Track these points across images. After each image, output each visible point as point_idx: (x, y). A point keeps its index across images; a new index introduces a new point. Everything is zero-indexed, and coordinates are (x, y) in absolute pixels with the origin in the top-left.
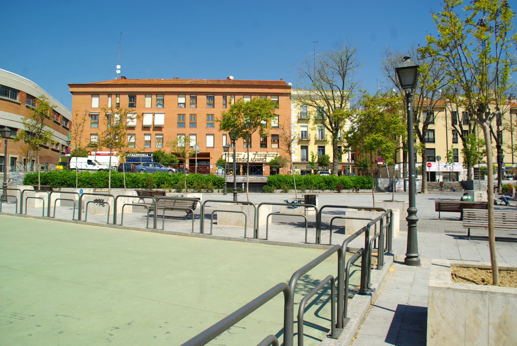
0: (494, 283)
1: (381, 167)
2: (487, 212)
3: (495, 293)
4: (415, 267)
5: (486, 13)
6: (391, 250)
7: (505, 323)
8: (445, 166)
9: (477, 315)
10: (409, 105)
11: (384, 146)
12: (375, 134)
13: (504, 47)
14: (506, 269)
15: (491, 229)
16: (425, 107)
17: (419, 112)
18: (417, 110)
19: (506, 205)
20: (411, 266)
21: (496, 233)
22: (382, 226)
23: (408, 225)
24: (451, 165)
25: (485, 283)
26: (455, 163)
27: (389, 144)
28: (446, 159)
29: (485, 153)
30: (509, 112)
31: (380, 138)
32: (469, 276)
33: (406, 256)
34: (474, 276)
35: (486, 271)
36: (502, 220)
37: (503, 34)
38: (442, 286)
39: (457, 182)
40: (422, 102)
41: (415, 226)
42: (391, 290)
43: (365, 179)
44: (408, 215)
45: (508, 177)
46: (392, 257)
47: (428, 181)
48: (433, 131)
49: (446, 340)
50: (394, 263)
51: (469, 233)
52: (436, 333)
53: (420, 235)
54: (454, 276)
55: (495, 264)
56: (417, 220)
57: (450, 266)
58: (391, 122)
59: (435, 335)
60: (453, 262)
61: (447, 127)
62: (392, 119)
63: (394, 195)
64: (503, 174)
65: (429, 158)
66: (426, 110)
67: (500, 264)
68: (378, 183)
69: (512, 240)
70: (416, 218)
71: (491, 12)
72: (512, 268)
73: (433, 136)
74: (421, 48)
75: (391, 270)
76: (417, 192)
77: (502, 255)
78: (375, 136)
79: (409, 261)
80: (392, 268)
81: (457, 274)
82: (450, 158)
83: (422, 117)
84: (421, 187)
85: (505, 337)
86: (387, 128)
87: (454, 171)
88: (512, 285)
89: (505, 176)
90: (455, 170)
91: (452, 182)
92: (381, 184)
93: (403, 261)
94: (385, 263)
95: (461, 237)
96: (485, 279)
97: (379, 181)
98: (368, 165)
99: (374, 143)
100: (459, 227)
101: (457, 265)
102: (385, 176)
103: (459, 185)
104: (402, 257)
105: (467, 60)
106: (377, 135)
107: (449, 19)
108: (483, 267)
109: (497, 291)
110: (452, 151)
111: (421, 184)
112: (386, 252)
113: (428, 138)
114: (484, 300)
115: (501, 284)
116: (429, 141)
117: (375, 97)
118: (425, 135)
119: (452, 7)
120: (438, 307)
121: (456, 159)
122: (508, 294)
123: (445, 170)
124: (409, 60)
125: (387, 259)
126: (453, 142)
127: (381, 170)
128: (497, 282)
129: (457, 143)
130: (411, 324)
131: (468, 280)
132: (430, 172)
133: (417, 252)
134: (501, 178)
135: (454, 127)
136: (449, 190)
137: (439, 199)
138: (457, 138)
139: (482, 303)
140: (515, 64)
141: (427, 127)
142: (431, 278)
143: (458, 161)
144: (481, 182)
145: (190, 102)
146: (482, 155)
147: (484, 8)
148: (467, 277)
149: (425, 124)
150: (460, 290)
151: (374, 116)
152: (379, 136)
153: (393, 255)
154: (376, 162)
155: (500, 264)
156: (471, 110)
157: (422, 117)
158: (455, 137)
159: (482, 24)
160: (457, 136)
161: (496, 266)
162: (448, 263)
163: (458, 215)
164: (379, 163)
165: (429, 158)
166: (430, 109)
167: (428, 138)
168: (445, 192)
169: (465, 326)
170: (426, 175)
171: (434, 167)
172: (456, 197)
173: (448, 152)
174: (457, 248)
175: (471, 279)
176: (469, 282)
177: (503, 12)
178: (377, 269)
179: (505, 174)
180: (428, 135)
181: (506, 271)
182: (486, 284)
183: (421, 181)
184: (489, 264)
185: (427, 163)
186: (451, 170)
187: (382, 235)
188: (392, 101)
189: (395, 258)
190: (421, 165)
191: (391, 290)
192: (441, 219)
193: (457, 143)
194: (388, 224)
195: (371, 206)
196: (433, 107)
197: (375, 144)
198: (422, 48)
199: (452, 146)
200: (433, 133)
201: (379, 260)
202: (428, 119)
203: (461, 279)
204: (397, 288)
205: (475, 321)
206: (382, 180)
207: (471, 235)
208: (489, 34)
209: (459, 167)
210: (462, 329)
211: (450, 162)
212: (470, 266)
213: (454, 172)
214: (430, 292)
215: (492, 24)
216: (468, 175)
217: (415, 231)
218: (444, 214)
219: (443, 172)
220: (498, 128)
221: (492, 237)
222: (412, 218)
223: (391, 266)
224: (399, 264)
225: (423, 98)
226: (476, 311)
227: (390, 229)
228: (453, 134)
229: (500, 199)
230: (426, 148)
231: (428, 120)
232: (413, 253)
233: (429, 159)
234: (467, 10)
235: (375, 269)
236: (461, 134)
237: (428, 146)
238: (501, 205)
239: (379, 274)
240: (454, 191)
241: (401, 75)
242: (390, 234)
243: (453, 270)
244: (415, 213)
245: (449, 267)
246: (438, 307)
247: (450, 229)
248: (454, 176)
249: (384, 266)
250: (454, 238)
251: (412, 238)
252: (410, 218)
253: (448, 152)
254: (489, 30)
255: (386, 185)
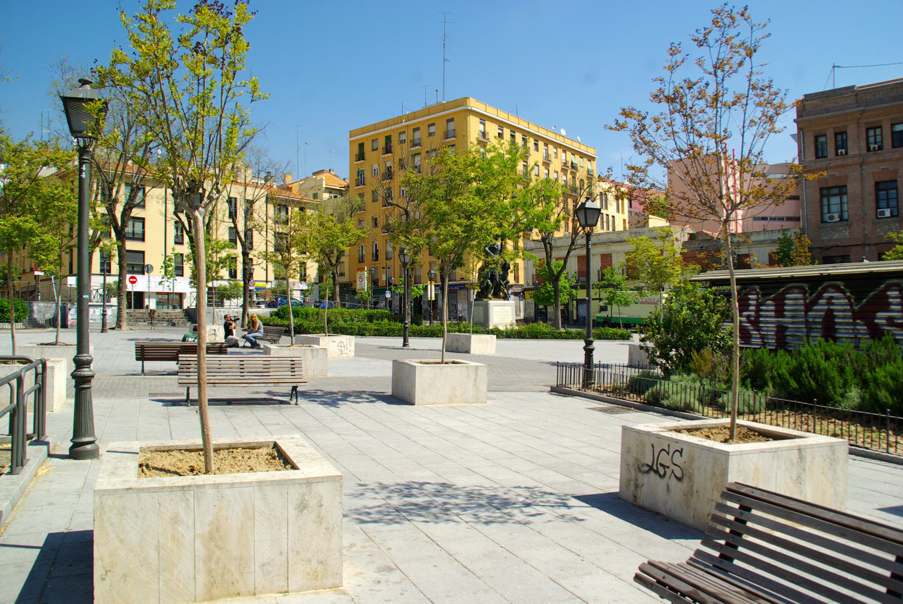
0: (207, 472)
1: (41, 281)
2: (196, 359)
3: (203, 486)
4: (89, 461)
5: (209, 34)
6: (43, 434)
7: (218, 530)
8: (160, 283)
9: (176, 526)
10: (84, 168)
11: (37, 241)
12: (18, 217)
13: (231, 94)
14: (227, 447)
15: (202, 384)
16: (127, 177)
17: (117, 184)
18: (114, 181)
19: (252, 347)
20: (81, 461)
21: (211, 393)
22: (21, 391)
23: (75, 387)
24: (171, 280)
25: (195, 472)
26: (178, 278)
27: (48, 237)
28: (163, 270)
29: (222, 263)
30: (264, 199)
31: (28, 226)
32: (170, 464)
33: (72, 444)
34: (179, 463)
35: (197, 453)
36: (290, 373)
37: (231, 74)
38: (119, 487)
39: (178, 310)
40: (124, 168)
41: (89, 388)
42: (37, 508)
43: (4, 303)
44: (75, 368)
45: (259, 303)
46: (45, 448)
47: (129, 307)
48: (142, 220)
49: (128, 578)
50: (49, 458)
51: (188, 394)
52: (110, 571)
53: (99, 404)
54: (144, 468)
55: (208, 439)
56: (93, 376)
57: (139, 451)
58: (53, 197)
59: (109, 573)
60: (144, 444)
61: (166, 216)
62: (56, 192)
63: (60, 334)
64: (251, 297)
65: (133, 268)
66: (130, 182)
67: (216, 440)
68: (32, 311)
69: (254, 402)
70: (90, 373)
71: (218, 34)
72: (235, 444)
73: (141, 229)
74: (99, 67)
75: (42, 472)
76: (108, 327)
77: (236, 427)
78: (17, 220)
79: (77, 451)
80: (43, 467)
81: (150, 464)
82: (170, 269)
83: (122, 194)
84: (116, 319)
85: (218, 552)
86: (45, 208)
87: (176, 291)
88: (233, 470)
89: (254, 302)
90: (178, 290)
91: (171, 310)
92: (39, 312)
93: (67, 453)
94: (29, 460)
95: (175, 403)
96: (195, 466)
97: (35, 308)
98: (14, 275)
99: (15, 233)
100: (173, 387)
101: (151, 449)
102: (49, 298)
103: (182, 315)
104: (65, 447)
105: (176, 105)
106: (22, 218)
107: (150, 28)
108: (193, 448)
109: (206, 483)
110: (173, 258)
111: (116, 313)
112: (34, 439)
113: (133, 233)
114: (187, 499)
115: (217, 472)
116: (134, 238)
117: (21, 145)
118: (126, 226)
119: (158, 10)
120: (112, 524)
121: (180, 271)
122: (221, 484)
123: (160, 289)
124: (88, 87)
125: (33, 452)
126: (176, 243)
127: (41, 286)
128: (211, 468)
129: (182, 243)
130: (71, 565)
131: (168, 471)
132: (135, 293)
133: (93, 435)
134: (247, 304)
135: (177, 216)
136: (165, 324)
137: (147, 339)
138: (182, 236)
139: (184, 505)
140: (247, 124)
141: (131, 211)
142: (103, 475)
143: (182, 275)
144: (216, 310)
145: (896, 189)
146: (217, 266)
147: (208, 26)
148: (167, 467)
149: (127, 207)
150: (149, 490)
151: (20, 182)
152: (26, 221)
153: (47, 444)
154: (32, 270)
155: (216, 440)
156: (176, 187)
157: (122, 194)
158: (179, 233)
159: (197, 48)
160: (182, 232)
161: (209, 443)
162: (135, 446)
163: (172, 365)
164: (36, 273)
165: (133, 268)
166: (137, 181)
167: (133, 233)
168: (159, 327)
169: (158, 548)
170: (125, 297)
171: (141, 284)
172: (175, 336)
173: (167, 259)
174: (166, 421)
175: (172, 469)
176: (169, 474)
177: (234, 39)
178: (10, 473)
179: (255, 299)
180: (134, 227)
181: (227, 449)
182: (197, 474)
183: (115, 309)
184: (199, 442)
185: (128, 276)
186: (170, 289)
187: (21, 408)
188: (57, 158)
189: (51, 450)
190: (117, 279)
191: (37, 508)
192: (145, 375)
193: (182, 243)
194: (38, 386)
195: (8, 353)
196: (143, 178)
197: (18, 236)
198: (102, 67)
199: (173, 250)
200: (141, 224)
201: (15, 456)
202: (131, 198)
203: (157, 472)
204: (50, 504)
205: (173, 537)
206: (42, 304)
207: (190, 398)
208: (210, 69)
209: (183, 285)
210: (153, 554)
211: (169, 276)
212: (172, 448)
213: (176, 294)
214: (97, 499)
215: (219, 53)
216: (198, 298)
217: (88, 396)
218: (150, 365)
219: (158, 293)
220: (246, 225)
221: (203, 398)
222: (82, 373)
223: (42, 465)
224: (58, 459)
225: (126, 161)
226: (176, 520)
227: (41, 396)
228: (177, 228)
229: (244, 337)
230: (127, 249)
231: (132, 200)
232: (85, 436)
233: (133, 269)
234: (183, 21)
235: (6, 474)
236: (188, 229)
237: (130, 245)
238: (244, 347)
239: (13, 483)
240: (174, 325)
241: (70, 110)
242: (41, 404)
243: (143, 458)
244: (88, 363)
245: (138, 453)
246: (112, 524)
247: (159, 390)
248: (175, 299)
249: (25, 467)
250: (164, 405)
251: (83, 409)
252: (79, 373)
253: (167, 259)
254: (214, 61)
255: (49, 316)
